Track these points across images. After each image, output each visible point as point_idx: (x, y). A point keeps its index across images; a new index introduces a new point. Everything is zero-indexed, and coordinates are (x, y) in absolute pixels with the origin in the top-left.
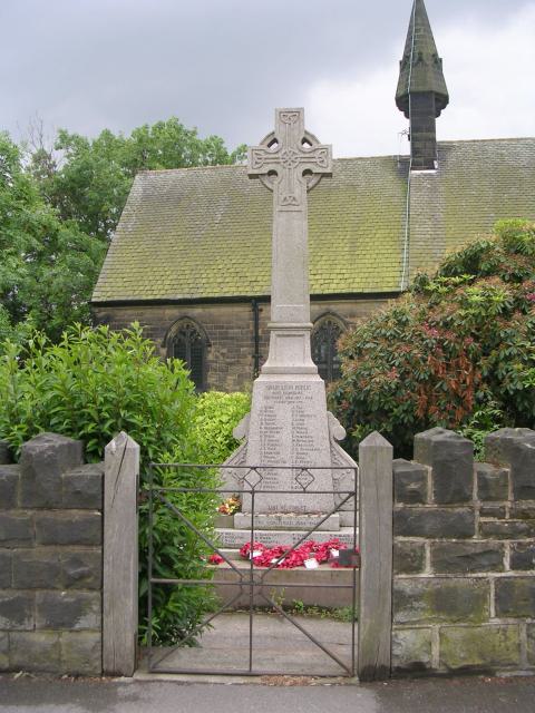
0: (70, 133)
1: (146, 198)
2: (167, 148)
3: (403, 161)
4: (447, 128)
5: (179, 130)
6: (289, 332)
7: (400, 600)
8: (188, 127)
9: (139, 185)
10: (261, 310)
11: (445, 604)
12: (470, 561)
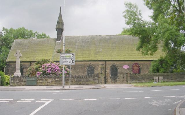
0: (5, 28)
1: (16, 44)
2: (22, 34)
3: (56, 39)
4: (65, 34)
5: (24, 29)
6: (17, 69)
7: (11, 83)
8: (26, 28)
9: (15, 41)
10: (128, 23)
11: (13, 83)
12: (15, 81)
